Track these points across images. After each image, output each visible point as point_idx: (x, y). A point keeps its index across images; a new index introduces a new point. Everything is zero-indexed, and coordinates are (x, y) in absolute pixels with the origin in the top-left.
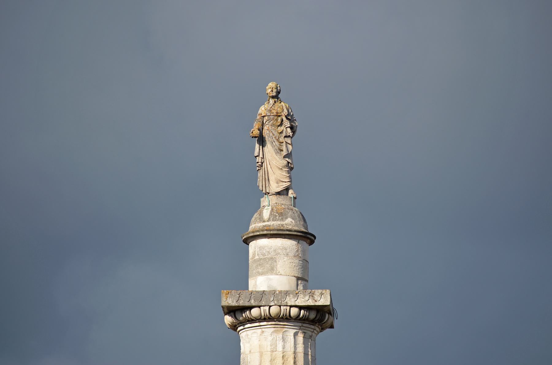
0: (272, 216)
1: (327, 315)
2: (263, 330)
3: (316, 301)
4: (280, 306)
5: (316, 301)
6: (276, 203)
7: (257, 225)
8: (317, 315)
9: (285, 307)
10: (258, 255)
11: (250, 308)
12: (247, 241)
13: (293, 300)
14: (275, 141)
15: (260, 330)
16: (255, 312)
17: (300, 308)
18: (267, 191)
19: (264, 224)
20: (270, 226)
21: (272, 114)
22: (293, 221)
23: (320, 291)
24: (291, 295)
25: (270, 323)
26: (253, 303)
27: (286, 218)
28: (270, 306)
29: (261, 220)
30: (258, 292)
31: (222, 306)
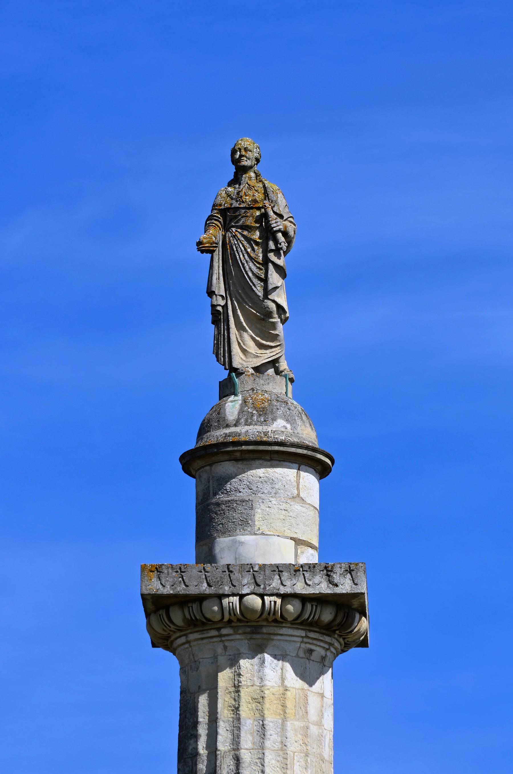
0: (244, 418)
1: (357, 616)
4: (262, 596)
22: (289, 426)
27: (274, 419)
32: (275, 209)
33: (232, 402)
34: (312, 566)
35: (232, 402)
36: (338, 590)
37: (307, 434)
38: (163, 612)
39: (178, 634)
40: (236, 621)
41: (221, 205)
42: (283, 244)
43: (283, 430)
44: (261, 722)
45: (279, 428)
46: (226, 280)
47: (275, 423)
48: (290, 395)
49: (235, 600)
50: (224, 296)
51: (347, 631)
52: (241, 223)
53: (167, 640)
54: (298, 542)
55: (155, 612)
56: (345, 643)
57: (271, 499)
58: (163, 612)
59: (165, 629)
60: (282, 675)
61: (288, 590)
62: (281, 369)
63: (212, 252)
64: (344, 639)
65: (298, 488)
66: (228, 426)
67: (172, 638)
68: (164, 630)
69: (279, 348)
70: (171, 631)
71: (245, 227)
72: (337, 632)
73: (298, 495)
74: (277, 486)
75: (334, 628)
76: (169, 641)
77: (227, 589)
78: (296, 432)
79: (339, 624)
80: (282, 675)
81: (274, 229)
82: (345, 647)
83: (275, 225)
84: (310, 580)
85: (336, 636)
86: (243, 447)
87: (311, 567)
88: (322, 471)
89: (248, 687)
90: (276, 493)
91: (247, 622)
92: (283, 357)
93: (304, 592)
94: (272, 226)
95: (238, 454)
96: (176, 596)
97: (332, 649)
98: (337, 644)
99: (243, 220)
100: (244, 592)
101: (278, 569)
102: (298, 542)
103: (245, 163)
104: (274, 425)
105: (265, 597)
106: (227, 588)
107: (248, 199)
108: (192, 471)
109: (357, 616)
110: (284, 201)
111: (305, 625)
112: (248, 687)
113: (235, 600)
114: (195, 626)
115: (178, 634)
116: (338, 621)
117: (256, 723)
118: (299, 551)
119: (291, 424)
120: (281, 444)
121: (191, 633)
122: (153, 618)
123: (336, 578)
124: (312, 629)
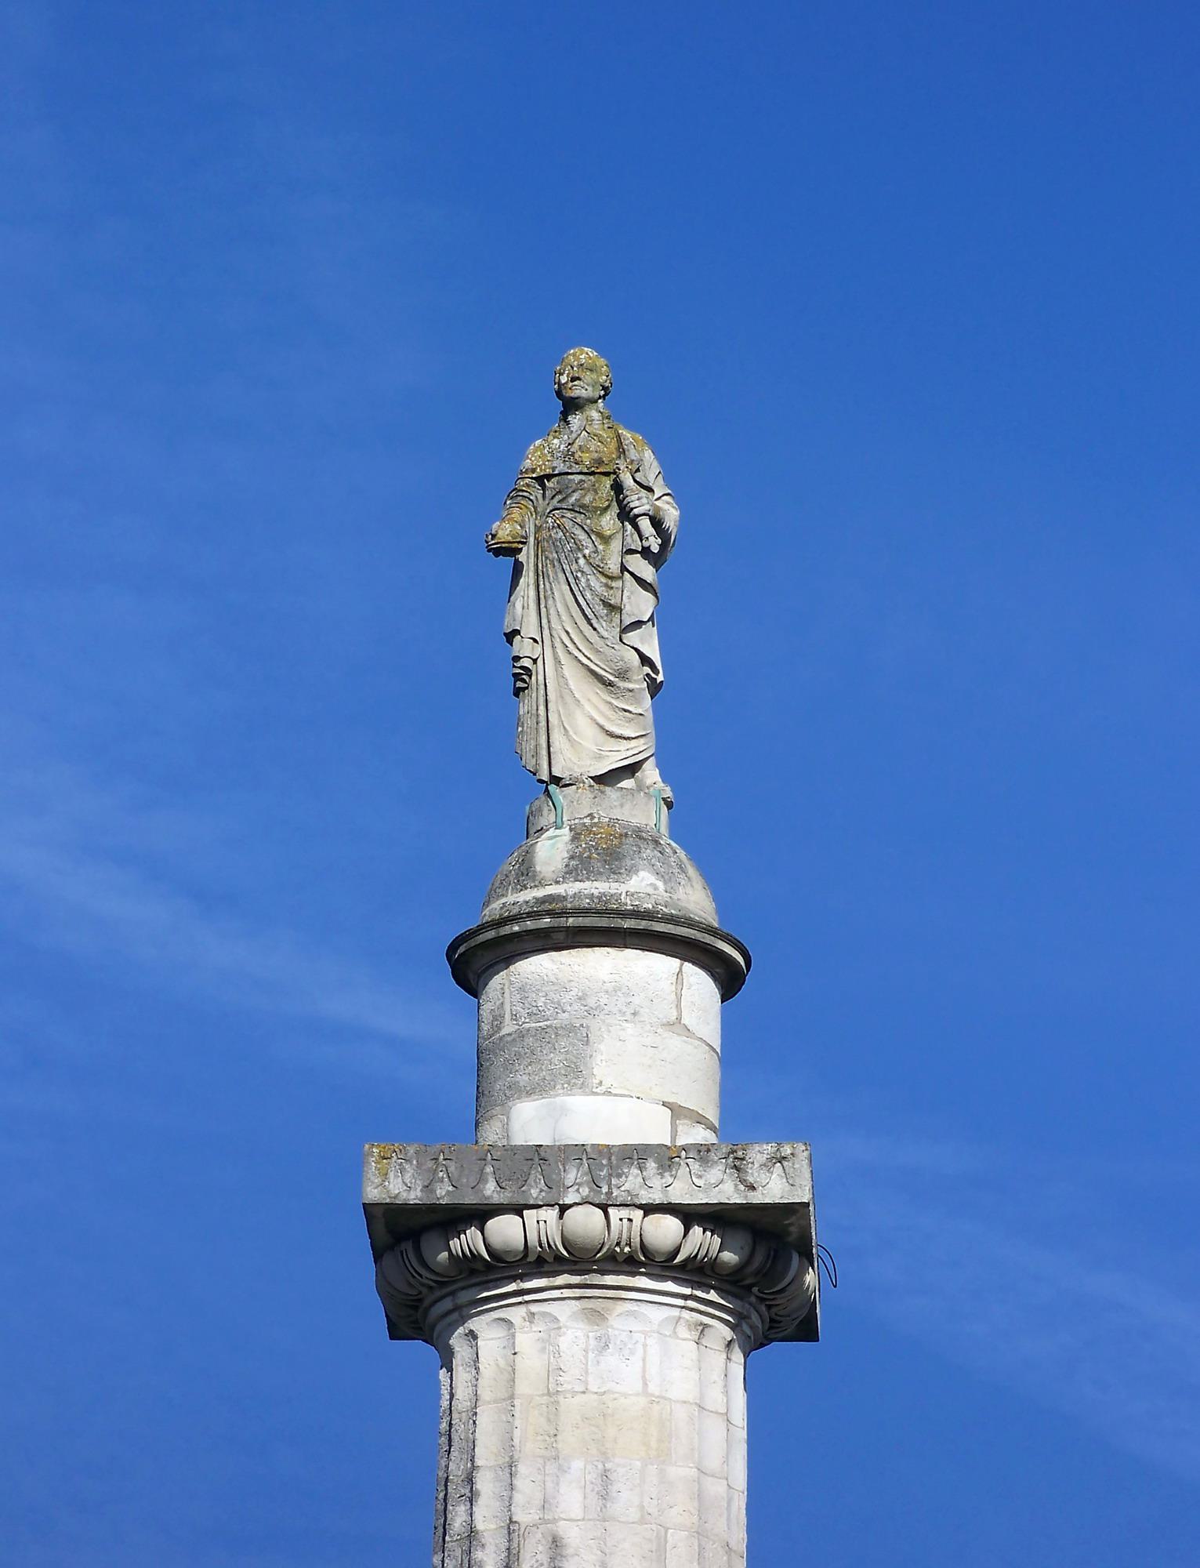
0: (578, 866)
1: (795, 1258)
2: (534, 1308)
3: (752, 1188)
4: (604, 1208)
5: (752, 1188)
6: (591, 815)
7: (511, 898)
8: (752, 1255)
9: (624, 1213)
10: (515, 1017)
11: (480, 1215)
12: (476, 959)
13: (656, 1182)
14: (587, 569)
15: (522, 1310)
16: (506, 1231)
17: (689, 1216)
18: (556, 773)
19: (540, 893)
20: (565, 898)
21: (576, 468)
22: (660, 885)
23: (769, 1148)
24: (651, 1165)
25: (561, 1280)
26: (491, 1191)
27: (632, 871)
28: (563, 1209)
29: (526, 873)
30: (514, 1150)
31: (368, 1208)
32: (638, 476)
33: (550, 838)
34: (703, 1148)
35: (550, 838)
36: (756, 1198)
37: (695, 899)
38: (408, 1246)
39: (438, 1293)
40: (551, 1260)
41: (534, 470)
42: (652, 539)
43: (650, 890)
44: (600, 1466)
45: (641, 886)
46: (543, 610)
47: (634, 877)
48: (664, 830)
49: (551, 1214)
50: (539, 639)
51: (743, 963)
52: (572, 500)
53: (416, 1308)
54: (677, 1111)
55: (391, 1247)
56: (772, 1320)
57: (625, 1025)
58: (408, 1246)
59: (411, 1280)
60: (644, 1371)
61: (657, 1198)
62: (649, 782)
63: (513, 552)
64: (769, 1307)
65: (678, 1006)
66: (542, 884)
67: (426, 1303)
68: (410, 1284)
69: (642, 741)
70: (423, 1285)
71: (580, 509)
72: (755, 1290)
73: (679, 1019)
74: (636, 1000)
75: (748, 1282)
76: (421, 1310)
77: (534, 1194)
78: (675, 897)
79: (757, 1273)
80: (644, 1371)
81: (636, 511)
82: (771, 1328)
83: (637, 503)
84: (700, 1177)
85: (753, 1299)
86: (571, 920)
87: (702, 1152)
88: (730, 981)
89: (574, 1393)
90: (634, 1014)
91: (575, 1263)
92: (652, 762)
93: (687, 1200)
94: (632, 505)
95: (561, 936)
96: (433, 1208)
97: (745, 1327)
98: (755, 1318)
99: (576, 496)
100: (568, 1201)
101: (636, 1155)
102: (677, 1111)
103: (580, 391)
104: (632, 882)
105: (611, 1210)
106: (534, 1192)
107: (587, 459)
108: (471, 976)
109: (795, 1258)
110: (655, 464)
111: (691, 1271)
112: (574, 1393)
113: (551, 1214)
114: (473, 1272)
115: (438, 1293)
116: (757, 1263)
117: (589, 1467)
118: (680, 1128)
119: (665, 883)
120: (648, 915)
121: (463, 1289)
122: (388, 1260)
123: (754, 1175)
124: (703, 1280)
